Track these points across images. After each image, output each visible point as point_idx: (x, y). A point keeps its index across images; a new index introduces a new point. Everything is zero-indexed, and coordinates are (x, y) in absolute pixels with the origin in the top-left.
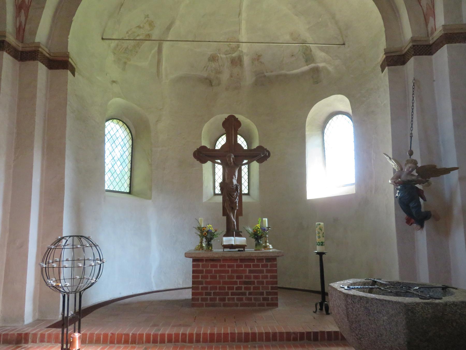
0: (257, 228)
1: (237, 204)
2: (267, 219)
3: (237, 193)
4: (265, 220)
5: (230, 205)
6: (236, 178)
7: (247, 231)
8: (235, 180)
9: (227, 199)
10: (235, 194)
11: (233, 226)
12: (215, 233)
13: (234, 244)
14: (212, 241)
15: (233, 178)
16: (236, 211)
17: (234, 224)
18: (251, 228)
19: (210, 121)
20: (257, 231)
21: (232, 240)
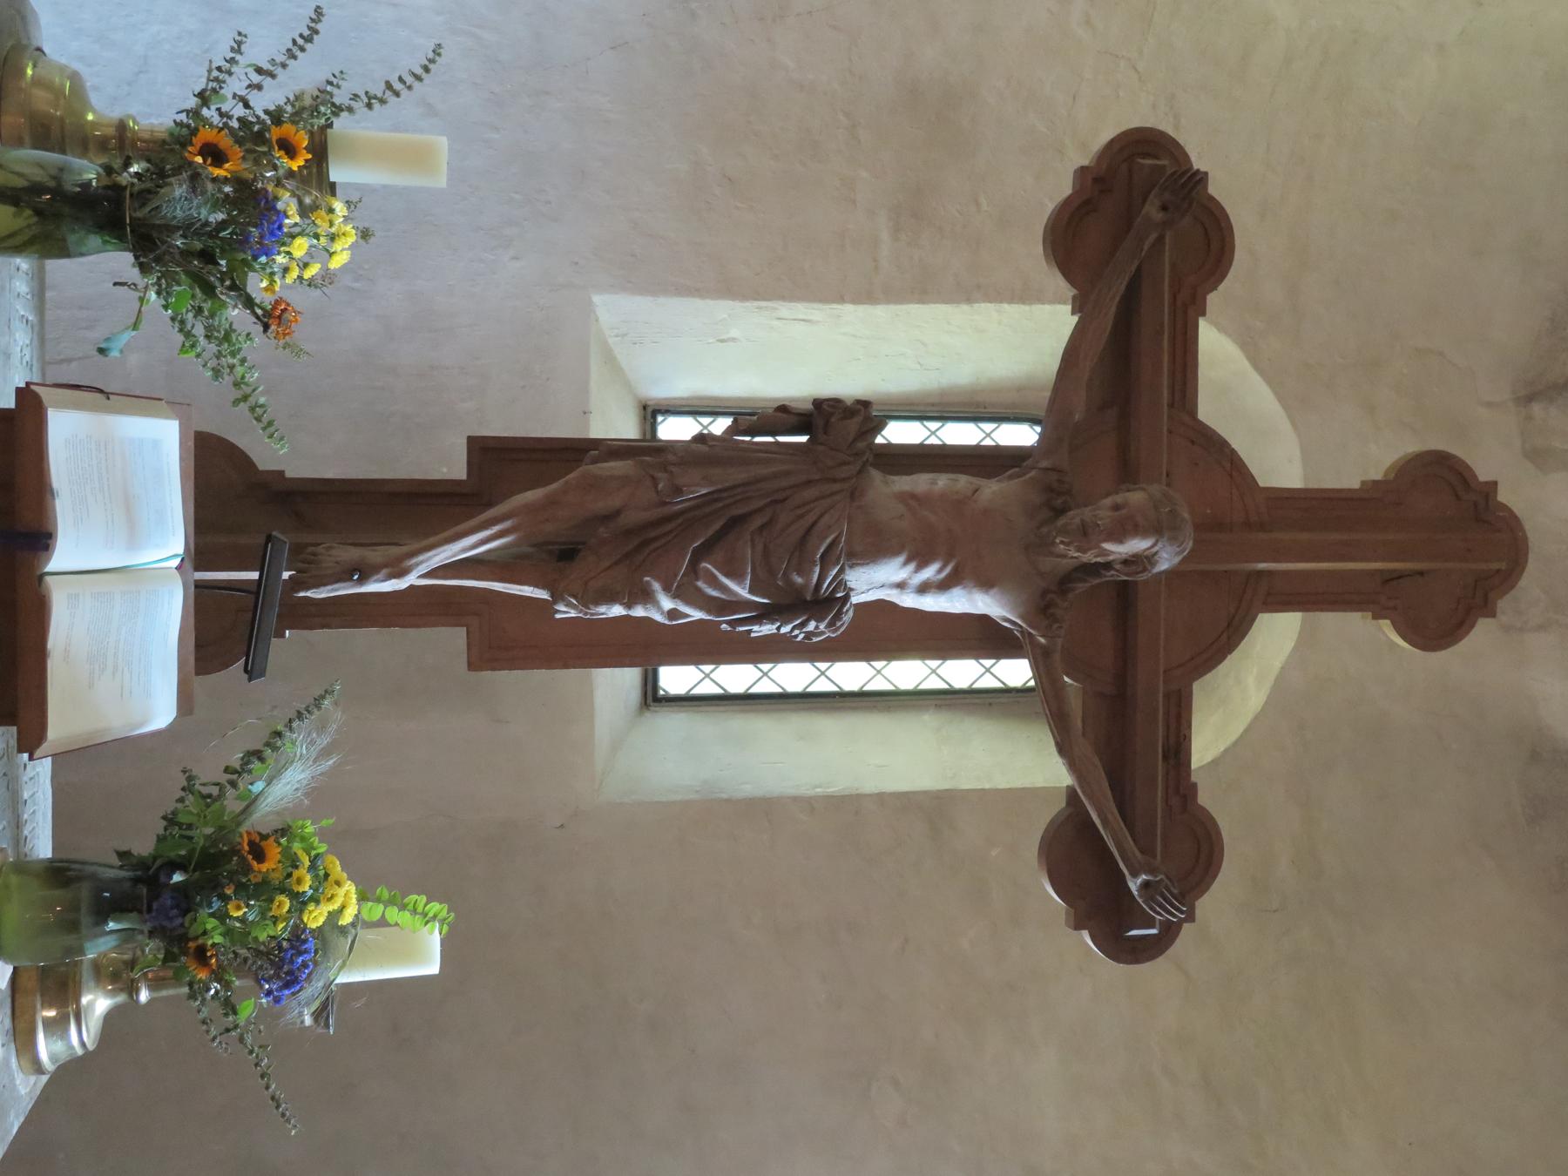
0: (306, 887)
1: (617, 610)
2: (433, 968)
3: (748, 605)
4: (411, 954)
5: (608, 517)
6: (908, 600)
7: (275, 749)
8: (901, 586)
9: (678, 491)
10: (742, 591)
11: (350, 554)
12: (235, 314)
13: (61, 558)
14: (121, 262)
15: (919, 568)
16: (527, 591)
17: (364, 572)
18: (318, 797)
19: (1255, 377)
20: (264, 891)
21: (133, 530)
